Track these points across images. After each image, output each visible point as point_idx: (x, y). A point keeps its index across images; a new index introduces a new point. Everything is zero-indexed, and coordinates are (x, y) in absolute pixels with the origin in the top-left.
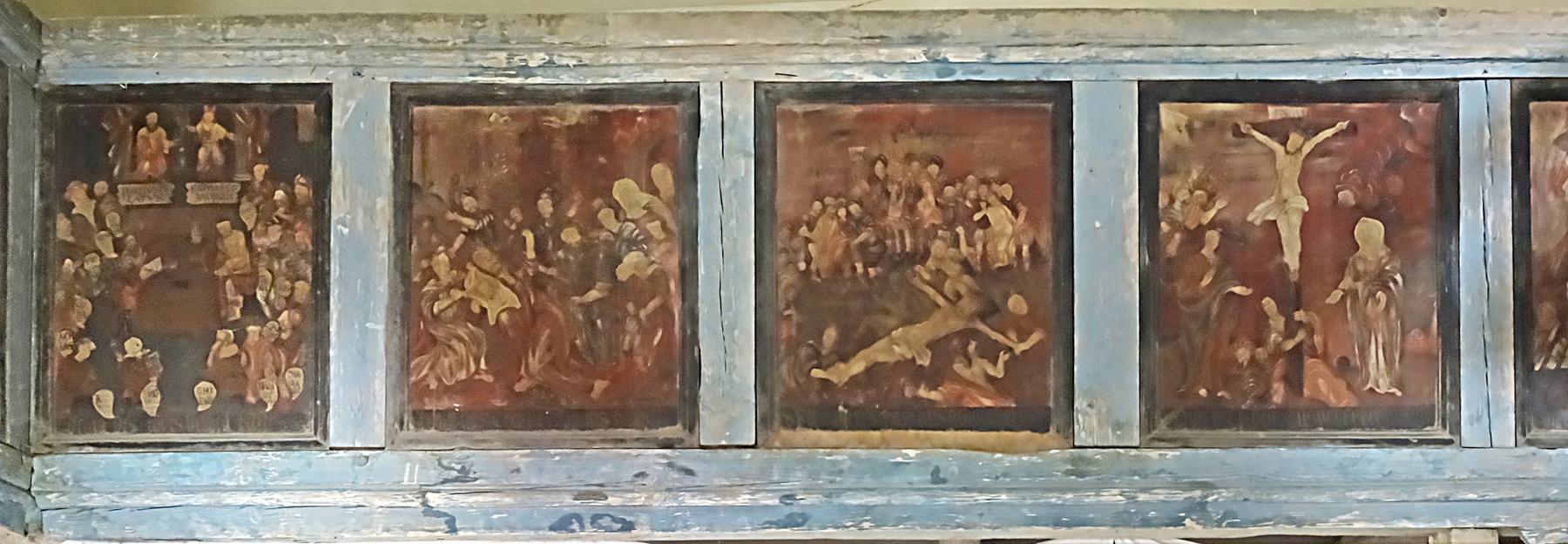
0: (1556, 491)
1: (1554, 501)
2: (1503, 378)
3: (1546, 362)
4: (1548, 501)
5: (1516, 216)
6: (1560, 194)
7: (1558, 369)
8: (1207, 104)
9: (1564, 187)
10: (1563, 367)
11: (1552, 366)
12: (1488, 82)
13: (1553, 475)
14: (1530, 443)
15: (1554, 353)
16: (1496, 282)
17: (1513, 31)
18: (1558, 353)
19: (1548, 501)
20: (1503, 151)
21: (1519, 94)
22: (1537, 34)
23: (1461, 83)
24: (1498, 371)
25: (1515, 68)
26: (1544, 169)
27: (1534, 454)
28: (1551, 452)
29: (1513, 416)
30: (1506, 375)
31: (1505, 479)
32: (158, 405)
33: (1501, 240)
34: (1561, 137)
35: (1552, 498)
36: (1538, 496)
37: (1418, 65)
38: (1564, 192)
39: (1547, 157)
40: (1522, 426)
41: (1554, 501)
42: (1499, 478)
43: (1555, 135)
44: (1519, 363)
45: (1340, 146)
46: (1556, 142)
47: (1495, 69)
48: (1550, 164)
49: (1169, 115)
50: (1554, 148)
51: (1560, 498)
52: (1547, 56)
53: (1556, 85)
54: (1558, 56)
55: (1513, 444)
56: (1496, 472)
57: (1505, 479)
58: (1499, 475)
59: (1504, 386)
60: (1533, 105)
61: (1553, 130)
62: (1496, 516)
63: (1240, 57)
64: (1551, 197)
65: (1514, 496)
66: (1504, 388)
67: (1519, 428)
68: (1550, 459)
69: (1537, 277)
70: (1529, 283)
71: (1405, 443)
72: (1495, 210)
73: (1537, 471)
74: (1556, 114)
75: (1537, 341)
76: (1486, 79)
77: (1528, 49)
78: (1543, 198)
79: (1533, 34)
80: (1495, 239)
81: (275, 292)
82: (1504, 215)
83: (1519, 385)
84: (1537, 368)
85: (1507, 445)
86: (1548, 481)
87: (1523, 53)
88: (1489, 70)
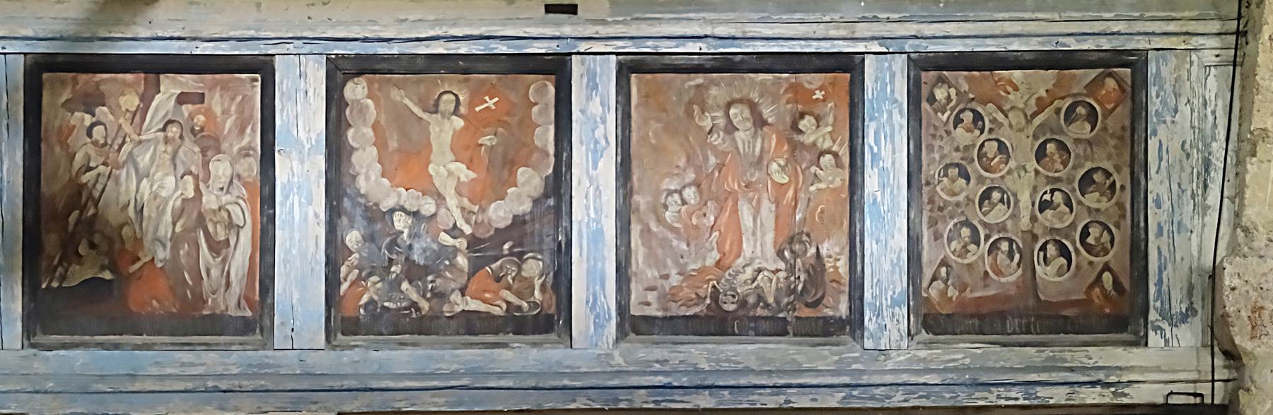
0: (51, 384)
1: (51, 392)
2: (13, 293)
3: (50, 282)
4: (46, 392)
5: (27, 164)
6: (65, 146)
7: (60, 287)
8: (526, 76)
9: (69, 141)
10: (64, 285)
11: (55, 284)
12: (7, 56)
13: (51, 371)
14: (33, 346)
15: (57, 274)
16: (9, 217)
17: (22, 15)
18: (60, 274)
19: (46, 392)
20: (16, 112)
21: (31, 66)
22: (42, 18)
23: (573, 56)
24: (9, 289)
25: (28, 45)
26: (53, 127)
27: (35, 355)
28: (49, 353)
29: (19, 324)
30: (15, 291)
31: (12, 374)
32: (233, 315)
33: (13, 184)
34: (67, 101)
35: (49, 390)
36: (37, 388)
37: (723, 41)
38: (68, 146)
39: (56, 116)
40: (28, 332)
41: (51, 392)
42: (7, 374)
43: (63, 99)
44: (26, 281)
45: (236, 109)
46: (63, 105)
47: (12, 45)
48: (57, 123)
49: (356, 90)
50: (61, 111)
51: (56, 390)
52: (50, 36)
53: (60, 59)
54: (58, 36)
55: (19, 346)
56: (5, 369)
57: (12, 374)
58: (6, 372)
59: (13, 299)
60: (45, 76)
61: (61, 96)
62: (9, 404)
63: (989, 41)
64: (58, 149)
65: (18, 388)
66: (13, 302)
67: (25, 334)
68: (47, 359)
69: (45, 213)
70: (37, 219)
71: (116, 346)
72: (10, 160)
73: (37, 368)
74: (63, 83)
75: (44, 264)
76: (5, 54)
77: (33, 30)
78: (51, 148)
79: (39, 18)
80: (8, 182)
81: (710, 222)
82: (16, 164)
83: (26, 298)
84: (44, 286)
85: (15, 348)
86: (47, 377)
87: (30, 33)
88: (7, 47)
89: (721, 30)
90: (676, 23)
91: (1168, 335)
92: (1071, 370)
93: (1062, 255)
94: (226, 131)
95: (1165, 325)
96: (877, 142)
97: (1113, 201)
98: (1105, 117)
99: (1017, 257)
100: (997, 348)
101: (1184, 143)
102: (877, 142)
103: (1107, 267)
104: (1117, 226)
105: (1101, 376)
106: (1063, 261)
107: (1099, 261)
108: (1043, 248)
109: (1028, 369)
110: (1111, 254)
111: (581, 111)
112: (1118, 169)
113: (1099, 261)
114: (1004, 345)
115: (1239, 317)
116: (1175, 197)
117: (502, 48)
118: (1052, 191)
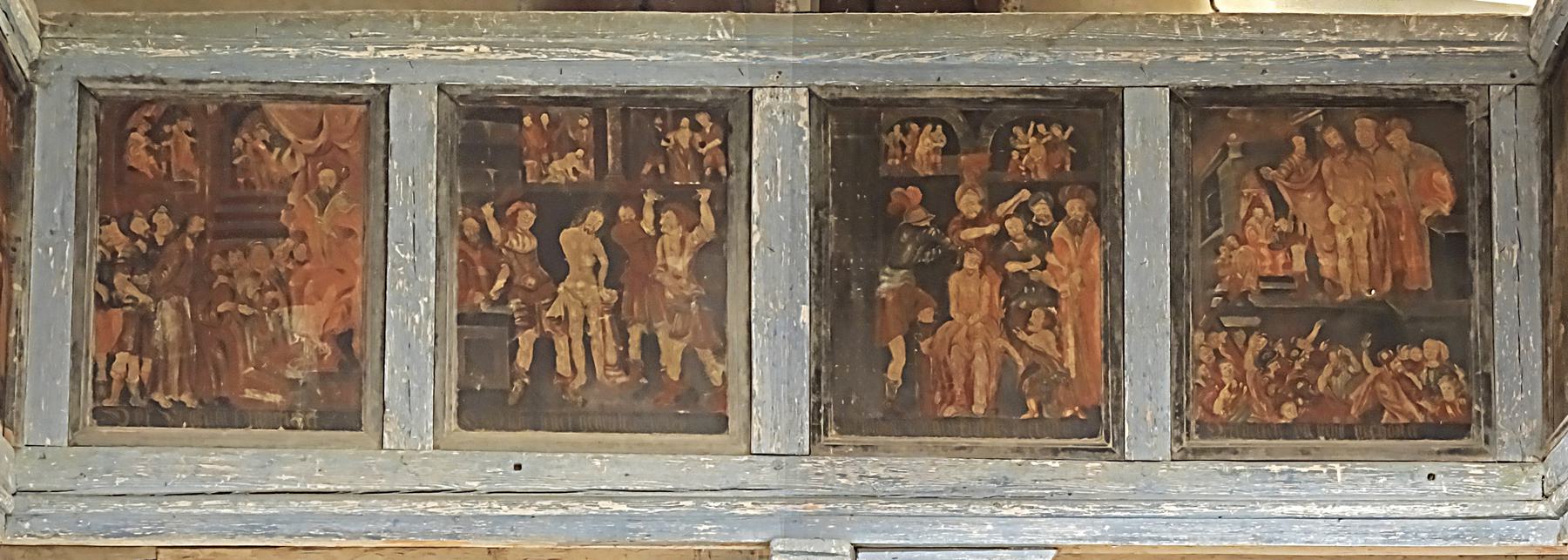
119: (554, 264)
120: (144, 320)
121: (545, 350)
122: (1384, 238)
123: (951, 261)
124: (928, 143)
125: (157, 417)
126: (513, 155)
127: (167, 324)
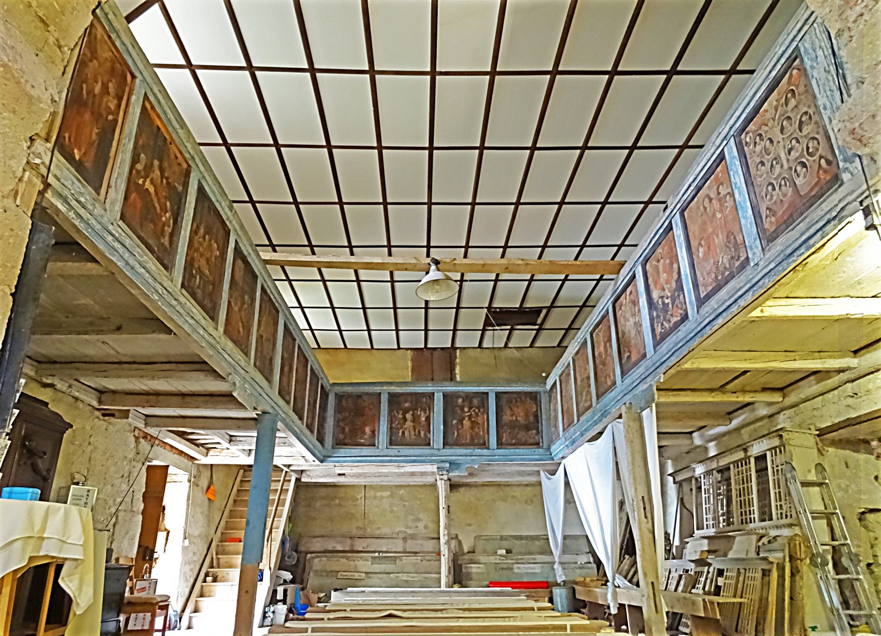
89: (691, 180)
90: (207, 402)
91: (851, 170)
92: (817, 222)
93: (803, 167)
94: (85, 97)
95: (848, 165)
96: (735, 179)
97: (813, 122)
98: (797, 89)
99: (788, 183)
100: (790, 233)
101: (825, 68)
102: (735, 179)
103: (821, 157)
104: (818, 133)
105: (828, 216)
106: (804, 169)
107: (816, 157)
108: (796, 171)
109: (802, 234)
110: (820, 149)
111: (427, 273)
112: (809, 107)
113: (816, 157)
114: (792, 229)
115: (847, 143)
116: (830, 97)
117: (661, 231)
118: (791, 142)
119: (405, 420)
120: (344, 429)
121: (403, 433)
122: (527, 415)
123: (464, 419)
124: (460, 400)
125: (346, 444)
126: (399, 403)
127: (347, 429)
